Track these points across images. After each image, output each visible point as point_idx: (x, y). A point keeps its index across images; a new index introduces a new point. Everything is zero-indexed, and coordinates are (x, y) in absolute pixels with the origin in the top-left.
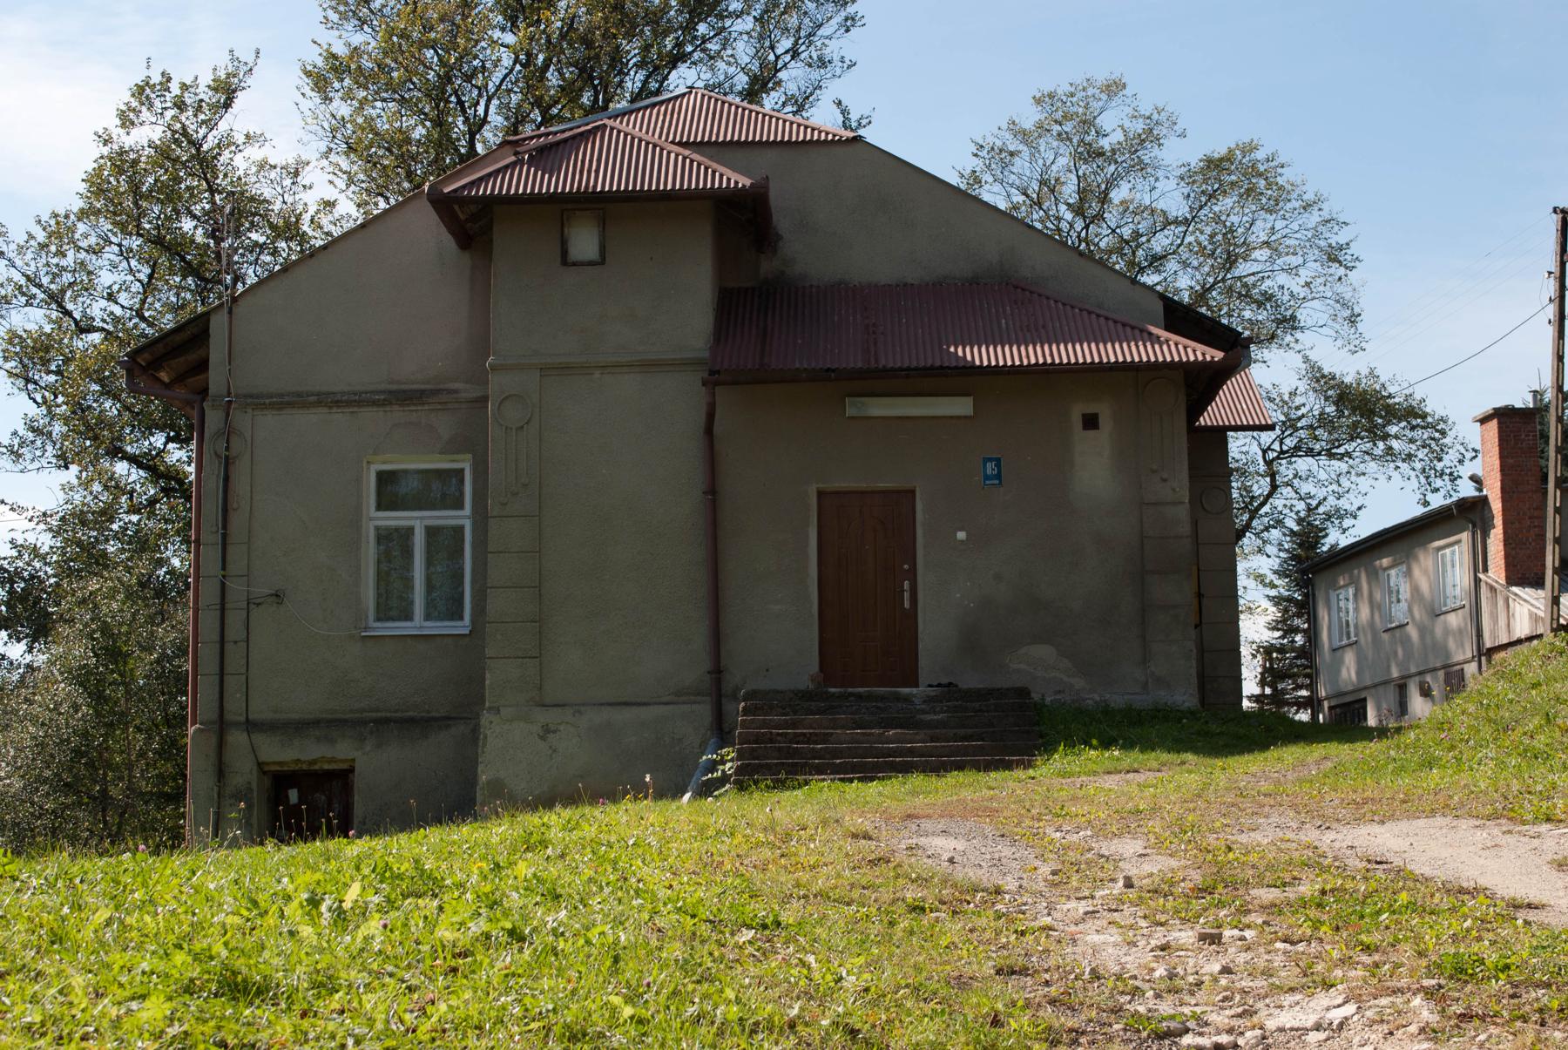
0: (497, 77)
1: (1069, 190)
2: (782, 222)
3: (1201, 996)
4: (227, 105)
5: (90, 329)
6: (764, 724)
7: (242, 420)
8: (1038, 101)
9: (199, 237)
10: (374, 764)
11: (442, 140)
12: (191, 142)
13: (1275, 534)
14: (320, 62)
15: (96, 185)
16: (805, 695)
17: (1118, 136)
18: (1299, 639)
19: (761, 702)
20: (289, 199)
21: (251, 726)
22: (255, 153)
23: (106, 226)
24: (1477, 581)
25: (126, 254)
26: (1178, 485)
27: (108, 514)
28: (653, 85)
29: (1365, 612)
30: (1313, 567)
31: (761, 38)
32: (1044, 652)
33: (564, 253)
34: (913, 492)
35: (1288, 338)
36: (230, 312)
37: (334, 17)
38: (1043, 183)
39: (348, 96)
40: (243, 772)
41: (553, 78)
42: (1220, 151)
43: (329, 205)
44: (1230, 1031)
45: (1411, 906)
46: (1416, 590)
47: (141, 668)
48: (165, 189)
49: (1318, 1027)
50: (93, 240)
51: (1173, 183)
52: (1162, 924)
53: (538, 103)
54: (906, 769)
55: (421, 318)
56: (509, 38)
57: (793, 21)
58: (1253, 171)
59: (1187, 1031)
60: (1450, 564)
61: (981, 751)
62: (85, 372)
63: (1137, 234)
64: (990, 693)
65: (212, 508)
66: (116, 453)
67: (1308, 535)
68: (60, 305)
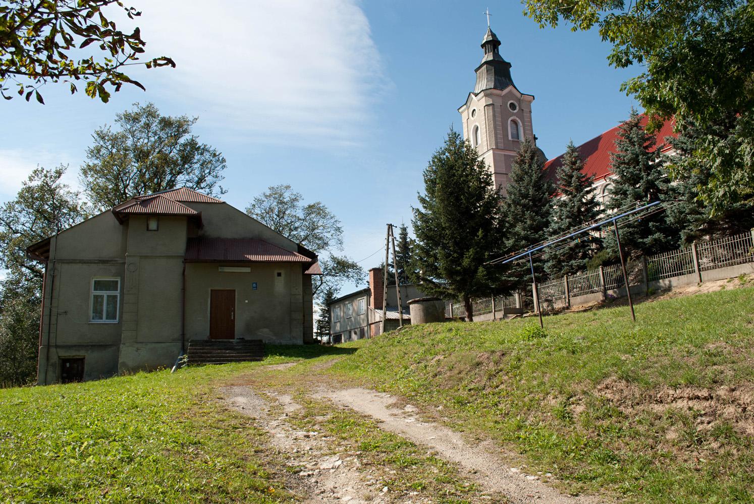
0: (132, 175)
1: (276, 211)
2: (204, 222)
3: (305, 459)
4: (59, 177)
5: (17, 232)
6: (195, 349)
7: (58, 266)
8: (270, 189)
9: (49, 210)
10: (91, 358)
11: (117, 189)
12: (48, 186)
13: (322, 294)
14: (85, 167)
15: (21, 195)
16: (207, 342)
17: (288, 199)
18: (326, 319)
19: (195, 343)
20: (74, 201)
21: (57, 346)
22: (67, 190)
23: (23, 206)
24: (368, 308)
25: (28, 213)
26: (300, 289)
27: (18, 282)
28: (173, 179)
29: (342, 314)
30: (331, 302)
31: (201, 169)
32: (266, 330)
33: (148, 228)
34: (234, 291)
35: (327, 248)
36: (56, 238)
37: (90, 156)
38: (270, 208)
39: (92, 176)
40: (54, 359)
41: (147, 176)
42: (312, 204)
43: (85, 203)
44: (312, 470)
45: (354, 423)
46: (354, 309)
47: (27, 323)
48: (41, 199)
49: (333, 468)
50: (20, 209)
51: (301, 211)
52: (295, 429)
53: (143, 182)
54: (231, 361)
55: (109, 242)
56: (136, 165)
57: (209, 165)
58: (319, 209)
59: (301, 470)
60: (362, 303)
61: (249, 356)
62: (15, 245)
63: (292, 222)
64: (255, 341)
65: (49, 282)
66: (22, 265)
67: (329, 294)
68: (9, 226)
